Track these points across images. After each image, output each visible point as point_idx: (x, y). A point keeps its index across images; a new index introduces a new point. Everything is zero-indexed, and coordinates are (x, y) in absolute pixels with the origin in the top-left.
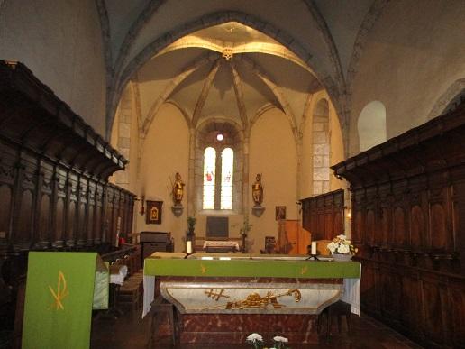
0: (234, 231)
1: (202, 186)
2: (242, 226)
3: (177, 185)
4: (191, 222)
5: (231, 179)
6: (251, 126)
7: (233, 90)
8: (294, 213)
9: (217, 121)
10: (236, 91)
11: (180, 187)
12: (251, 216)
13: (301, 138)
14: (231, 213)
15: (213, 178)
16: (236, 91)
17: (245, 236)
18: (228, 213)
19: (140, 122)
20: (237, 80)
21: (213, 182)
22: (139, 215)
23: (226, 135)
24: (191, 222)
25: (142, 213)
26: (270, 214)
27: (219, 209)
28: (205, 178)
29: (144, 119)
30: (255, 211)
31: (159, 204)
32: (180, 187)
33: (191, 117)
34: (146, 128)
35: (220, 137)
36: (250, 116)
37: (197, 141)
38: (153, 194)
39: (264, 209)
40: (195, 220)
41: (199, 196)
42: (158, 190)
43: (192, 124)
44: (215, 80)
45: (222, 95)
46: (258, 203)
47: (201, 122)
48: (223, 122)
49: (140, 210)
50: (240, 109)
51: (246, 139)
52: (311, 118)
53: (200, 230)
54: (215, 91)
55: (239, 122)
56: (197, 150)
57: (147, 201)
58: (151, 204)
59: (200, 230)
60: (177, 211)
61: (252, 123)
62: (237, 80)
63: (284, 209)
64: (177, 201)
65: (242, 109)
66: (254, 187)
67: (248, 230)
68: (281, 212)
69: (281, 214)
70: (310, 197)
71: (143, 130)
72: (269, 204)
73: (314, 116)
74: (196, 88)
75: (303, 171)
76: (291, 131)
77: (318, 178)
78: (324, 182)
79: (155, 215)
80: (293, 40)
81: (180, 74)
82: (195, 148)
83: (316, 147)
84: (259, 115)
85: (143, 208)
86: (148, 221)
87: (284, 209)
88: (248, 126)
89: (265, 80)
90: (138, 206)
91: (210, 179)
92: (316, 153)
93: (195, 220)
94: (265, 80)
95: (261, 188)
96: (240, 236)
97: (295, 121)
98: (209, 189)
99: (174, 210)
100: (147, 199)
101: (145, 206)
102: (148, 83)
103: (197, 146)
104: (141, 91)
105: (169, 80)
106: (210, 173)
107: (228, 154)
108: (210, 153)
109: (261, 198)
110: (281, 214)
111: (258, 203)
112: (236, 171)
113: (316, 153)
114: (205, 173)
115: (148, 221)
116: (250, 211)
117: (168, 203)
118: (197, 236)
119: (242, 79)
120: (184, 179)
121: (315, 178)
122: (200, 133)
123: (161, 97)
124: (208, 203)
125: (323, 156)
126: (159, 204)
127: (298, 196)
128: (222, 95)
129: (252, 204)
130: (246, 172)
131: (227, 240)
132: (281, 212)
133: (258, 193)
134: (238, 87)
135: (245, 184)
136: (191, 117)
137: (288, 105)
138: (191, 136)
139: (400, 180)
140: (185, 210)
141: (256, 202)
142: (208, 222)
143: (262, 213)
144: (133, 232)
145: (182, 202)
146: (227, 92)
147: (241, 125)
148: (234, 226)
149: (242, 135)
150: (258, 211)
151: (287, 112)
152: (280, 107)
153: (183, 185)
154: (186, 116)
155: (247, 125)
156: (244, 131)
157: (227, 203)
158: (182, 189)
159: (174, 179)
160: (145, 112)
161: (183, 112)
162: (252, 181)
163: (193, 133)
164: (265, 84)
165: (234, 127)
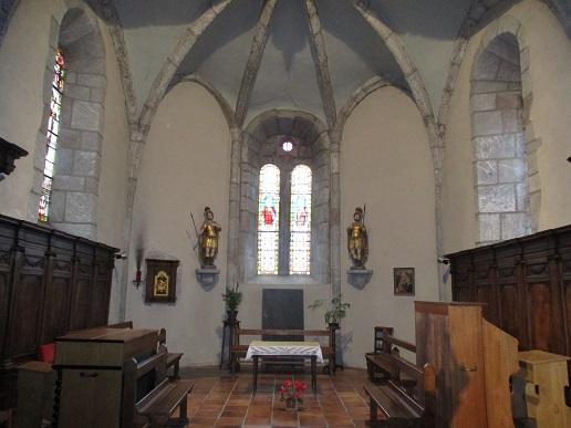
0: (314, 319)
1: (256, 233)
2: (331, 307)
3: (206, 231)
4: (233, 300)
5: (309, 219)
6: (343, 123)
7: (307, 51)
8: (433, 284)
9: (281, 115)
10: (314, 50)
11: (212, 233)
12: (346, 289)
13: (441, 135)
14: (309, 281)
15: (276, 219)
16: (314, 50)
17: (334, 326)
18: (301, 281)
19: (132, 110)
20: (315, 24)
21: (275, 226)
22: (131, 287)
23: (298, 142)
24: (233, 300)
25: (138, 281)
26: (383, 282)
27: (288, 275)
28: (261, 219)
29: (140, 106)
30: (353, 277)
31: (171, 266)
32: (212, 233)
33: (232, 104)
34: (144, 122)
35: (288, 147)
36: (341, 102)
37: (245, 150)
38: (158, 248)
39: (369, 275)
40: (240, 295)
41: (248, 251)
42: (172, 239)
43: (235, 119)
44: (270, 29)
45: (288, 65)
46: (359, 263)
47: (253, 116)
48: (292, 116)
49: (132, 276)
50: (322, 88)
51: (335, 146)
52: (467, 86)
53: (250, 315)
54: (273, 54)
55: (321, 116)
56: (245, 167)
57: (148, 260)
58: (155, 265)
59: (250, 315)
60: (206, 277)
61: (346, 115)
62: (315, 24)
63: (411, 273)
64: (207, 260)
65: (325, 89)
66: (350, 232)
67: (342, 314)
68: (405, 280)
69: (404, 283)
70: (471, 246)
71: (139, 125)
72: (382, 263)
73: (473, 81)
74: (238, 49)
75: (449, 193)
76: (421, 122)
77: (490, 207)
78: (502, 215)
79: (162, 287)
80: (443, 147)
81: (203, 12)
82: (241, 163)
83: (482, 142)
84: (356, 101)
85: (139, 274)
86: (150, 299)
87: (411, 273)
88: (337, 120)
89: (371, 19)
90: (125, 271)
91: (269, 221)
92: (482, 155)
93: (240, 295)
94: (371, 19)
95: (363, 234)
96: (324, 327)
97: (429, 104)
98: (268, 239)
99: (201, 276)
100: (147, 255)
101: (143, 269)
102: (142, 30)
103: (245, 159)
104: (128, 47)
105: (185, 27)
106: (270, 210)
107: (302, 176)
108: (269, 176)
109: (364, 252)
110: (404, 283)
111: (359, 263)
112: (315, 205)
113: (482, 155)
114: (261, 209)
115: (150, 299)
116: (345, 278)
117: (189, 267)
118: (242, 327)
119: (325, 24)
120: (220, 218)
121: (483, 208)
122: (251, 137)
123: (170, 61)
124: (267, 262)
125: (498, 160)
126: (171, 266)
127: (440, 242)
128: (288, 65)
129: (348, 264)
130: (335, 206)
131: (300, 339)
132: (405, 280)
133: (358, 243)
134: (318, 40)
135: (335, 227)
136: (232, 104)
137: (415, 70)
138: (233, 142)
139: (368, 394)
140: (222, 277)
141: (356, 261)
142: (265, 299)
143: (367, 281)
144: (113, 319)
145: (216, 263)
146: (298, 56)
147: (325, 121)
148: (315, 306)
149: (327, 138)
150: (360, 274)
151: (418, 95)
152: (406, 89)
153: (217, 230)
154: (224, 106)
155: (335, 121)
156: (329, 132)
157: (300, 262)
158: (216, 238)
159: (200, 219)
160: (141, 100)
161: (219, 99)
162: (347, 220)
163: (236, 136)
164: (369, 26)
165: (313, 125)
